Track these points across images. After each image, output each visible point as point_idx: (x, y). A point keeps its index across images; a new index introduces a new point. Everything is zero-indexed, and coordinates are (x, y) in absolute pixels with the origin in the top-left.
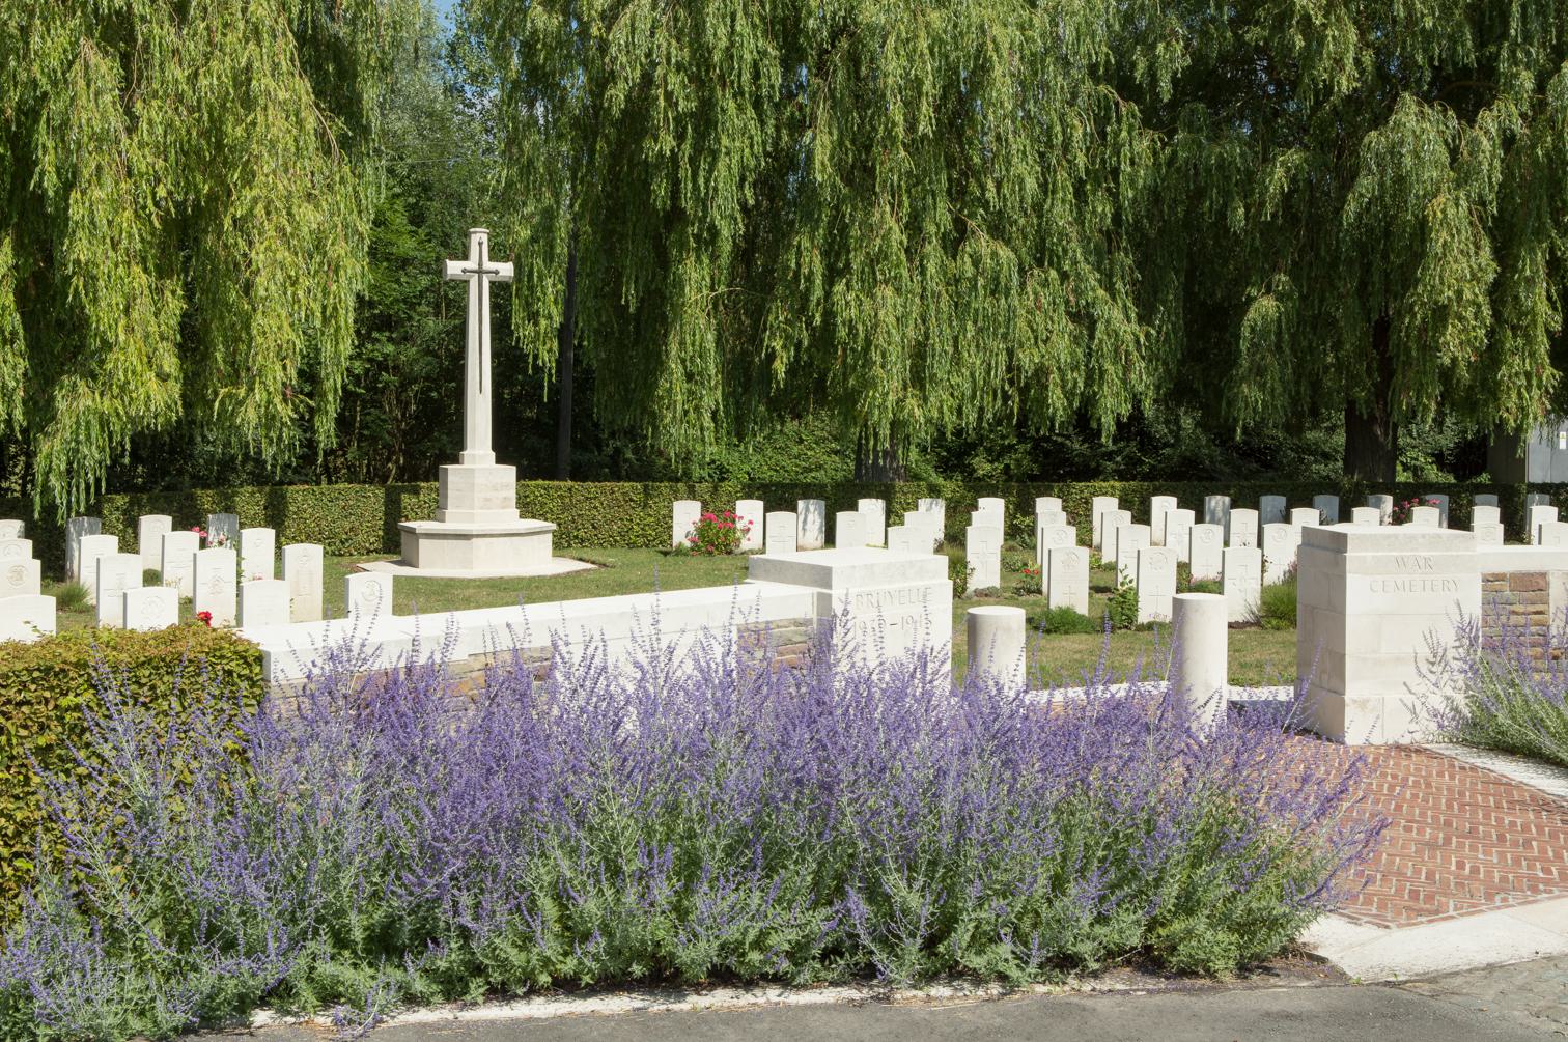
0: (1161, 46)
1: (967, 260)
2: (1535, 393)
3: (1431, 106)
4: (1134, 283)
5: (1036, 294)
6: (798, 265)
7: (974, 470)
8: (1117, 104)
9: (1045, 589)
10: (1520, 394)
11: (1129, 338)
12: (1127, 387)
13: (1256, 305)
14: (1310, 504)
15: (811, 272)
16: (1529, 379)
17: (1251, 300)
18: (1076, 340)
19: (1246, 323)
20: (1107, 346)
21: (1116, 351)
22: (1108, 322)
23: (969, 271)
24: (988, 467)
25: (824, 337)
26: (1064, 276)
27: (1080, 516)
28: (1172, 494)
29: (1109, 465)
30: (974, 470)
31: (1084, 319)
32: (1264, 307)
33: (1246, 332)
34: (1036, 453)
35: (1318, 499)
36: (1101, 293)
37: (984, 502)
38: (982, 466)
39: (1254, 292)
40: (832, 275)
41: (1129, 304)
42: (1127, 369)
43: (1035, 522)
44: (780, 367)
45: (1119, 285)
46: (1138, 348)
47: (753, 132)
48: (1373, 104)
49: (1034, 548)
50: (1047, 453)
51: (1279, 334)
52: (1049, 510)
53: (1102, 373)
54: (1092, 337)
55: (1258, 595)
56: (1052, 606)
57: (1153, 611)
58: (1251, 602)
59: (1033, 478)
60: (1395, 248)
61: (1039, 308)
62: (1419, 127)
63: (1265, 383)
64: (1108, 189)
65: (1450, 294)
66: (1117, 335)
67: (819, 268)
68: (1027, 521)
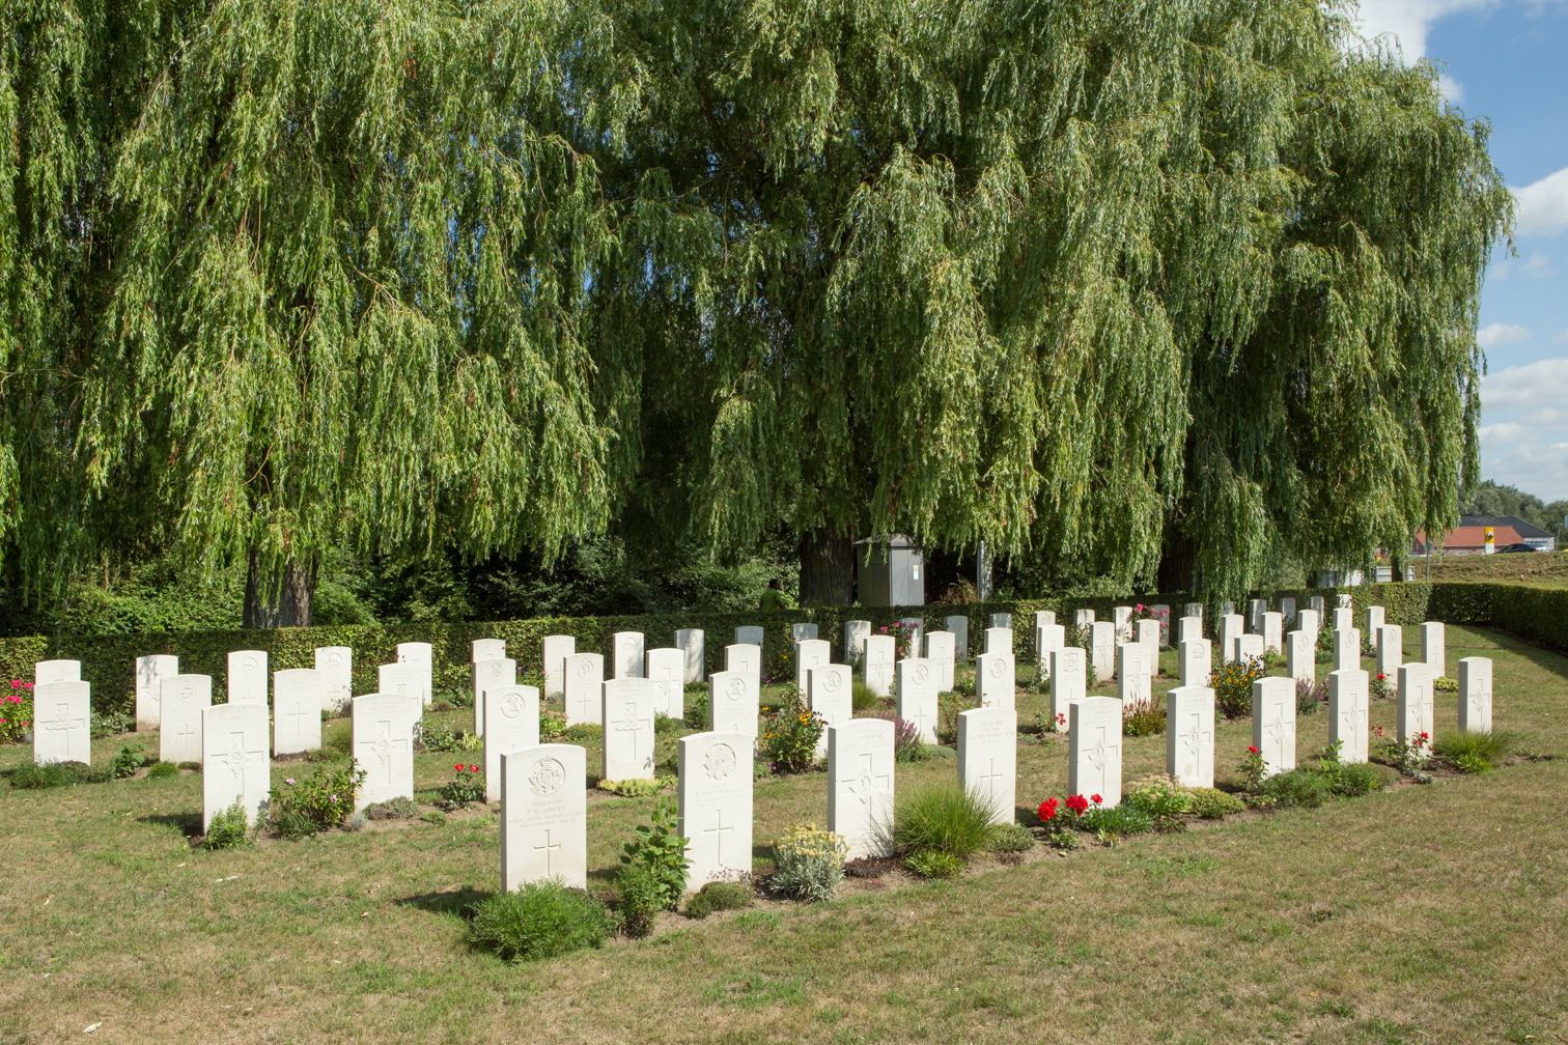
0: (615, 90)
1: (372, 331)
2: (1023, 495)
3: (930, 163)
4: (590, 375)
5: (468, 386)
6: (119, 325)
7: (412, 614)
8: (569, 158)
9: (492, 791)
10: (1009, 498)
11: (585, 441)
12: (578, 516)
13: (727, 406)
14: (943, 627)
15: (139, 338)
16: (1017, 481)
17: (720, 401)
18: (517, 444)
19: (718, 427)
20: (560, 449)
21: (569, 458)
22: (559, 424)
23: (374, 344)
24: (426, 611)
25: (157, 421)
26: (506, 367)
27: (529, 664)
28: (74, 655)
29: (546, 605)
30: (412, 614)
31: (535, 420)
32: (733, 411)
33: (716, 436)
34: (468, 584)
35: (951, 620)
36: (553, 384)
37: (405, 649)
38: (419, 609)
39: (724, 393)
40: (176, 339)
41: (585, 402)
42: (582, 485)
43: (472, 670)
44: (99, 474)
45: (572, 379)
46: (597, 455)
47: (63, 149)
48: (865, 156)
49: (472, 705)
50: (483, 595)
51: (755, 439)
52: (490, 655)
53: (551, 486)
54: (539, 440)
55: (890, 808)
56: (513, 886)
57: (717, 869)
58: (880, 819)
59: (468, 619)
60: (893, 325)
61: (471, 404)
62: (913, 184)
63: (741, 496)
64: (557, 265)
65: (951, 376)
66: (571, 439)
67: (150, 330)
68: (462, 670)
